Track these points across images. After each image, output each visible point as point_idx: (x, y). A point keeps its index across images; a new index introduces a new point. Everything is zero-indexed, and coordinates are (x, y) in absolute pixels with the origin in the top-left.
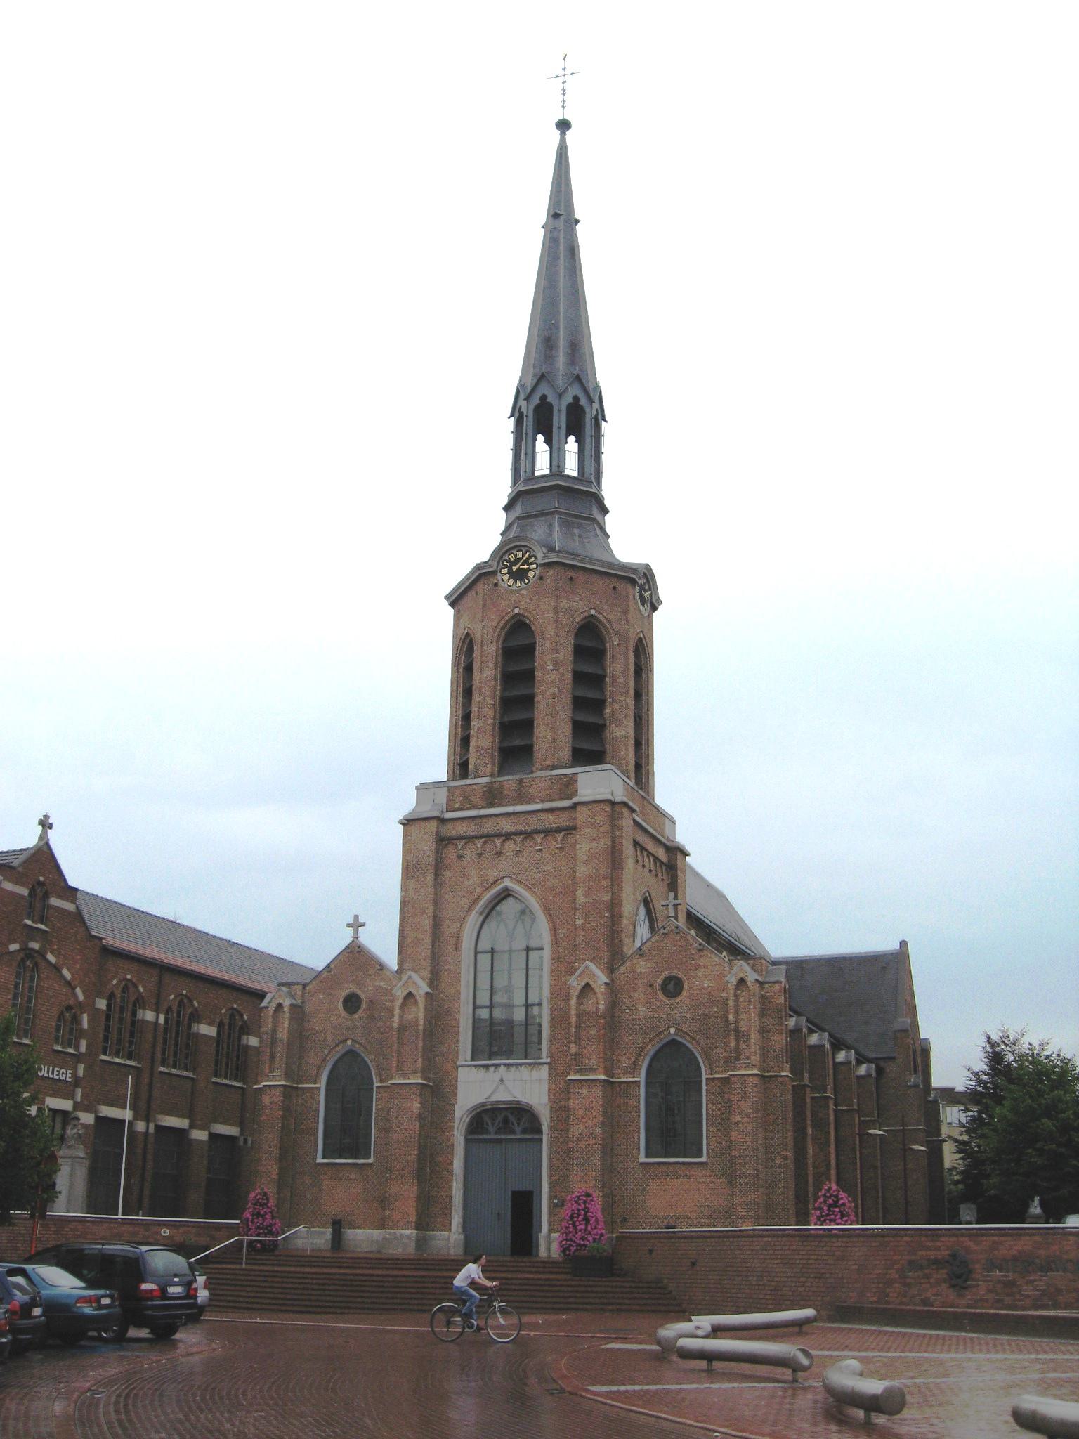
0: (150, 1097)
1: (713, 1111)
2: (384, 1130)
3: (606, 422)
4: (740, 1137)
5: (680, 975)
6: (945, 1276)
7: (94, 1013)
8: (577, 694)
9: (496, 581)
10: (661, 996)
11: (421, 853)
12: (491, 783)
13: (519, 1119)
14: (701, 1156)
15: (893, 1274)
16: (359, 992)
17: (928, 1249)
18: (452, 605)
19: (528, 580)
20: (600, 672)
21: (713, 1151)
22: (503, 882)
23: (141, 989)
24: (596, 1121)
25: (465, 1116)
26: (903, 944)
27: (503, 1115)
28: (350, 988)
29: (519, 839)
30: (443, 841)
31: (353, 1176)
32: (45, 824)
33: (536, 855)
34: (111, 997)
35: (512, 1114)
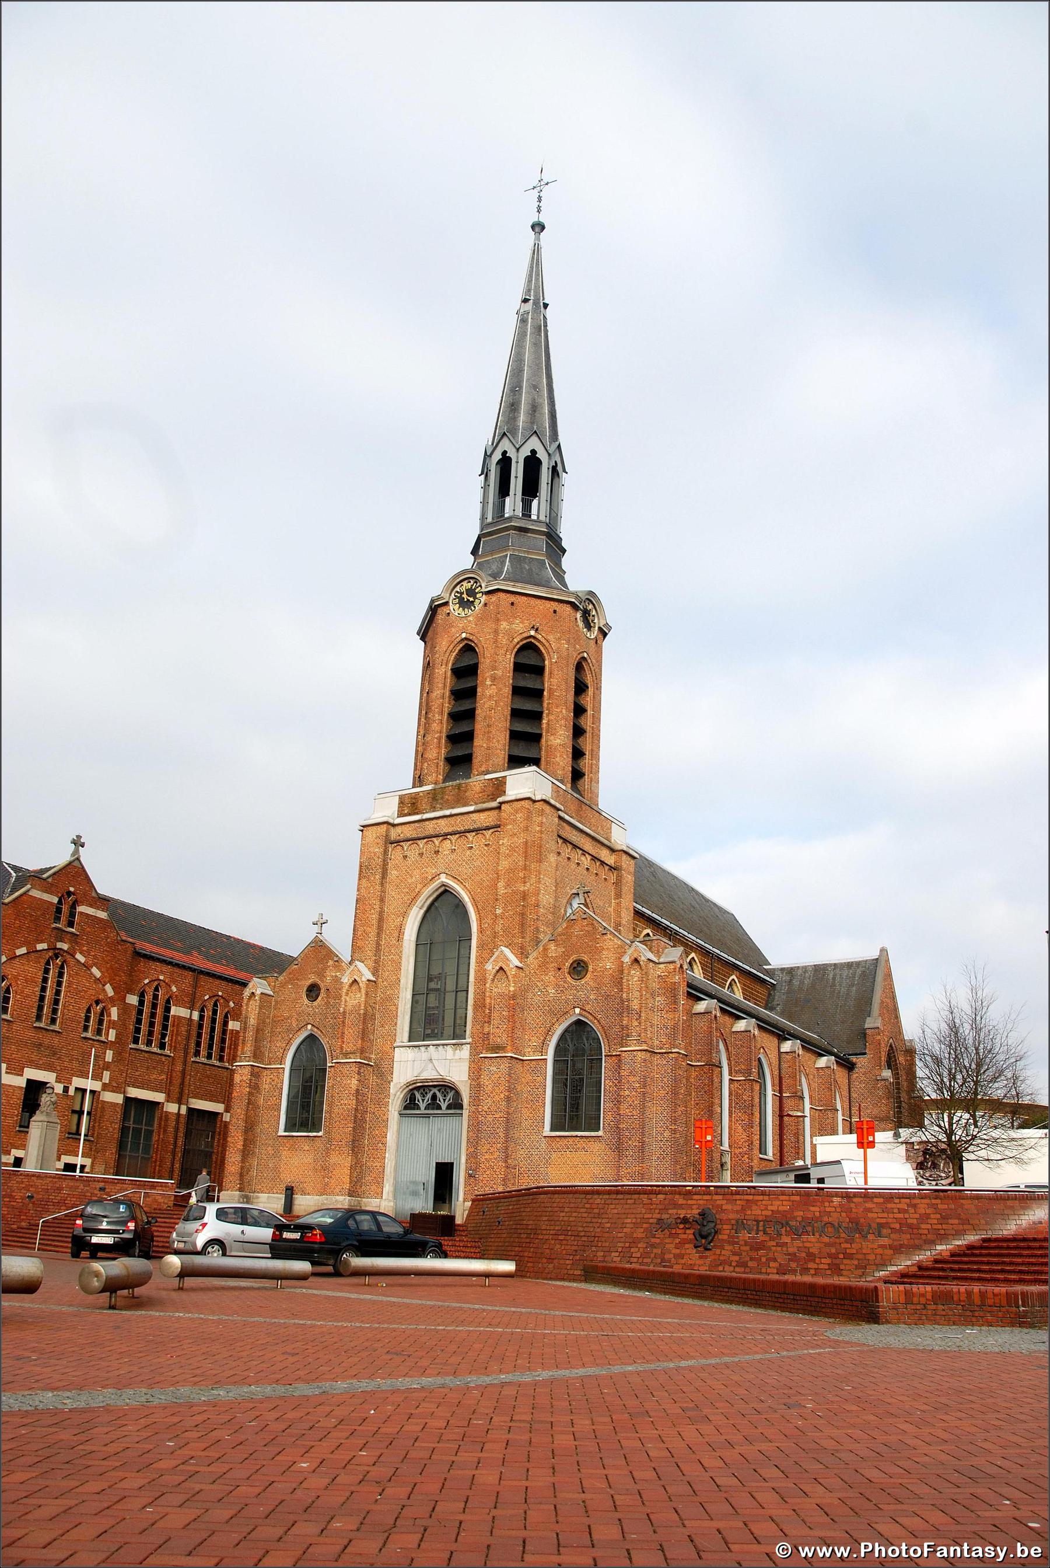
0: (182, 1083)
1: (610, 1086)
2: (331, 1105)
3: (567, 473)
4: (627, 1111)
5: (585, 958)
6: (691, 1237)
7: (125, 1008)
8: (515, 707)
9: (448, 611)
10: (569, 979)
11: (372, 854)
12: (434, 790)
13: (445, 1096)
14: (598, 1129)
15: (639, 1233)
16: (319, 982)
17: (681, 1207)
18: (423, 638)
19: (475, 607)
20: (538, 686)
21: (609, 1124)
22: (439, 879)
23: (174, 989)
24: (502, 1096)
25: (399, 1093)
26: (883, 951)
27: (432, 1092)
28: (312, 979)
29: (454, 838)
30: (391, 842)
31: (306, 1148)
32: (78, 843)
33: (468, 852)
34: (142, 995)
35: (439, 1091)
